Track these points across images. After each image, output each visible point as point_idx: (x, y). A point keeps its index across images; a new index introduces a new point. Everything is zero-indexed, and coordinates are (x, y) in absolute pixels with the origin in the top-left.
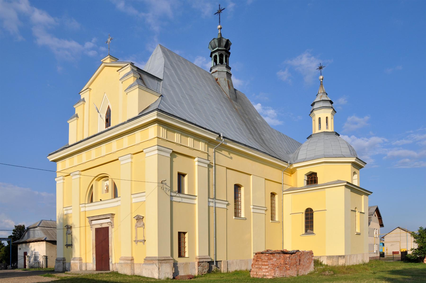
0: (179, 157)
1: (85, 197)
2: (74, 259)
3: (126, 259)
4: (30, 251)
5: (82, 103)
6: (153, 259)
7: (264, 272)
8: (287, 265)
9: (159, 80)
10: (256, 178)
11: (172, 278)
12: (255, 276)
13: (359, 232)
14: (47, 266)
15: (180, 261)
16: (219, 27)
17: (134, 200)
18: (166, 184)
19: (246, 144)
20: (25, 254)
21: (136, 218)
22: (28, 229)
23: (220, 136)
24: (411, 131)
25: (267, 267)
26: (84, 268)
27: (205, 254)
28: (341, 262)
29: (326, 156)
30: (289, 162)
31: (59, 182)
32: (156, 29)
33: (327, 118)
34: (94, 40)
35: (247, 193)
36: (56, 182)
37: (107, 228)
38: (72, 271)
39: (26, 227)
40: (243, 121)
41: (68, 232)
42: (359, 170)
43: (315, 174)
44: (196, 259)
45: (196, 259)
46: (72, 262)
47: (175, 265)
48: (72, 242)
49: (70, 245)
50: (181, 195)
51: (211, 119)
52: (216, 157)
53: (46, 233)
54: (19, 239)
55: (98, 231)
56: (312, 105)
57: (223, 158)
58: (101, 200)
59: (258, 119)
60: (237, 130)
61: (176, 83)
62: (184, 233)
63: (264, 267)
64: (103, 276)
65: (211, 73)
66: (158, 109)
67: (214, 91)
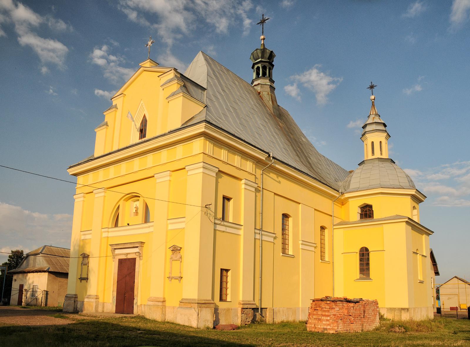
0: (225, 177)
1: (109, 220)
2: (89, 297)
3: (156, 300)
4: (27, 283)
5: (114, 109)
6: (191, 301)
7: (325, 325)
8: (351, 317)
9: (203, 89)
10: (306, 206)
11: (212, 327)
12: (313, 330)
13: (422, 280)
14: (46, 305)
15: (222, 306)
16: (262, 37)
17: (170, 227)
18: (209, 209)
19: (297, 167)
20: (21, 286)
21: (171, 249)
22: (28, 255)
23: (269, 155)
24: (447, 165)
25: (329, 318)
26: (100, 309)
27: (250, 298)
28: (405, 317)
29: (383, 186)
30: (340, 191)
31: (79, 201)
32: (170, 41)
33: (381, 142)
34: (105, 48)
35: (296, 225)
36: (74, 200)
37: (134, 259)
38: (85, 312)
39: (25, 254)
40: (288, 140)
41: (84, 263)
42: (418, 204)
43: (370, 207)
44: (240, 304)
45: (240, 304)
46: (86, 300)
47: (216, 311)
48: (87, 275)
49: (84, 279)
50: (226, 223)
51: (257, 137)
52: (264, 180)
53: (49, 262)
54: (15, 268)
55: (121, 262)
56: (364, 127)
57: (272, 182)
58: (128, 224)
59: (304, 140)
60: (284, 150)
61: (220, 93)
62: (227, 271)
63: (325, 318)
64: (127, 321)
65: (253, 85)
66: (206, 121)
67: (258, 105)
